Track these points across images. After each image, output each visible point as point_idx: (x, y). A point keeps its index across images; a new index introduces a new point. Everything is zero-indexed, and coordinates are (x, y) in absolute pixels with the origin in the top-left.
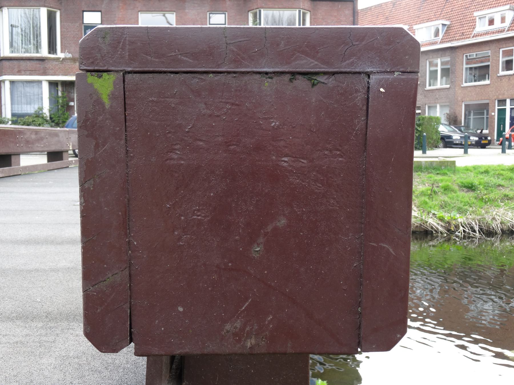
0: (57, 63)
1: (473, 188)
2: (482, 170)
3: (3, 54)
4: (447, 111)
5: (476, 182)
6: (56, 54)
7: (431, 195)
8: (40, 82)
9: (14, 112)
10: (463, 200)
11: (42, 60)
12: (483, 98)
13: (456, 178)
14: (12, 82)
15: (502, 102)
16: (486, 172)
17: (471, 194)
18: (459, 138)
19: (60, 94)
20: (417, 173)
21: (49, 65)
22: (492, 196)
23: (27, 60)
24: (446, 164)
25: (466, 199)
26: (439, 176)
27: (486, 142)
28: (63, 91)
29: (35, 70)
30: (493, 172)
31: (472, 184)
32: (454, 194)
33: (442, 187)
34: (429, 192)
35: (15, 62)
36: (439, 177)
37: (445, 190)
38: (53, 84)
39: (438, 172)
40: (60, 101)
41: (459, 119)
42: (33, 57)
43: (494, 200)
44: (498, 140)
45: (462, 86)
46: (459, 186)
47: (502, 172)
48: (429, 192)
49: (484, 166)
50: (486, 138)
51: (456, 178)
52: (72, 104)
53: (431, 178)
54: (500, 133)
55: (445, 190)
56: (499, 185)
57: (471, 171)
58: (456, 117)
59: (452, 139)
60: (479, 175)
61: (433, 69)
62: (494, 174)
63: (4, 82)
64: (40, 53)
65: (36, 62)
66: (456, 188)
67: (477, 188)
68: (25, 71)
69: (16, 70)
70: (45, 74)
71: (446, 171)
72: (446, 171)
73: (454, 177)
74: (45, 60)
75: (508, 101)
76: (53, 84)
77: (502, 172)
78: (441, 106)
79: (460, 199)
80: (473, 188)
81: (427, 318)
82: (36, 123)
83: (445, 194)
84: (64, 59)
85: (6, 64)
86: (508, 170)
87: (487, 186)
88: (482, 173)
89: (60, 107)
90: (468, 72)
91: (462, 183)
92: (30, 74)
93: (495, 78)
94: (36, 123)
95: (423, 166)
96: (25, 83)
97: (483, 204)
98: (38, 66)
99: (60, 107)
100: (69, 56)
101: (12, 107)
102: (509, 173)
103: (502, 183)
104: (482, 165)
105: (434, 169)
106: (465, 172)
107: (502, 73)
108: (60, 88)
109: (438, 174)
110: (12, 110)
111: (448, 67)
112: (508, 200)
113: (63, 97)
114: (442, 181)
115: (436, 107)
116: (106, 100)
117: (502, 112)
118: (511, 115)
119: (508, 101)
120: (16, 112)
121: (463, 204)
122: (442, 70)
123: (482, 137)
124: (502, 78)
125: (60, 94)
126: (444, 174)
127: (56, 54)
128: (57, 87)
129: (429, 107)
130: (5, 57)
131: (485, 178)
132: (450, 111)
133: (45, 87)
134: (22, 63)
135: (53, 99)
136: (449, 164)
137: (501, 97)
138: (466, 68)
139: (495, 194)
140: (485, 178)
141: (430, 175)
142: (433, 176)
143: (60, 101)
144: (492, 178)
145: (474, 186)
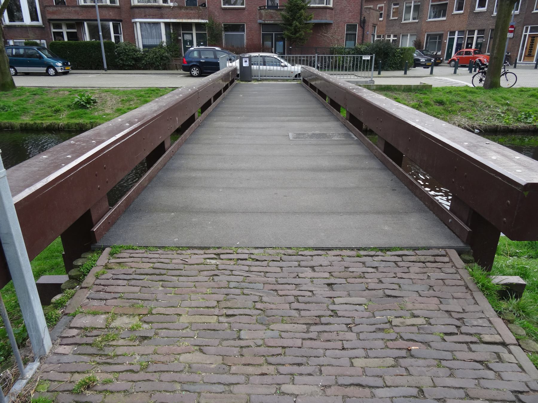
0: (170, 10)
1: (443, 103)
2: (448, 91)
3: (134, 3)
4: (414, 38)
5: (445, 100)
6: (168, 3)
7: (418, 107)
8: (158, 23)
9: (144, 44)
10: (436, 111)
11: (159, 7)
12: (440, 30)
13: (432, 97)
14: (141, 23)
15: (453, 33)
16: (450, 92)
17: (441, 107)
18: (424, 61)
19: (172, 31)
20: (409, 93)
21: (164, 11)
22: (454, 108)
23: (150, 7)
24: (426, 87)
25: (439, 111)
26: (422, 95)
27: (439, 61)
28: (173, 30)
29: (155, 15)
30: (454, 92)
31: (442, 101)
32: (431, 107)
33: (425, 103)
34: (417, 106)
35: (142, 9)
36: (422, 96)
37: (426, 104)
38: (167, 25)
39: (421, 92)
40: (173, 36)
41: (422, 44)
42: (153, 6)
43: (455, 111)
44: (447, 59)
45: (427, 21)
46: (434, 102)
47: (460, 92)
48: (417, 106)
49: (448, 87)
50: (439, 59)
51: (432, 97)
52: (180, 38)
53: (417, 96)
54: (449, 55)
55: (426, 104)
56: (458, 101)
57: (441, 92)
58: (420, 43)
59: (420, 61)
60: (445, 94)
61: (408, 5)
62: (455, 94)
63: (136, 23)
64: (158, 3)
65: (155, 9)
66: (432, 103)
67: (445, 103)
68: (149, 15)
69: (143, 15)
70: (162, 17)
71: (426, 92)
72: (426, 92)
73: (431, 96)
74: (161, 8)
75: (457, 33)
76: (167, 25)
77: (460, 92)
78: (411, 35)
79: (435, 110)
80: (443, 103)
81: (42, 40)
82: (161, 52)
83: (426, 107)
84: (174, 7)
85: (137, 10)
86: (463, 91)
87: (451, 102)
88: (448, 93)
89: (172, 40)
90: (434, 9)
91: (436, 100)
92: (153, 18)
93: (450, 16)
94: (161, 52)
95: (412, 88)
96: (152, 25)
97: (448, 113)
98: (157, 12)
99: (172, 40)
100: (176, 4)
101: (142, 41)
102: (464, 93)
103: (459, 99)
104: (446, 87)
105: (419, 90)
106: (437, 92)
107: (455, 12)
108: (171, 27)
109: (421, 93)
110: (142, 43)
111: (419, 4)
112: (463, 111)
113: (174, 33)
114: (424, 98)
115: (408, 35)
116: (526, 196)
117: (452, 40)
118: (457, 42)
119: (457, 33)
120: (146, 44)
121: (437, 113)
122: (414, 6)
123: (437, 57)
124: (455, 16)
125: (172, 31)
126: (425, 94)
127: (168, 3)
128: (170, 27)
129: (403, 35)
130: (136, 6)
131: (450, 97)
132: (416, 38)
133: (163, 27)
134: (146, 10)
135: (168, 35)
136: (428, 87)
137: (452, 30)
138: (432, 5)
139: (456, 107)
140: (450, 97)
141: (417, 94)
142: (418, 95)
143: (173, 36)
144: (454, 97)
145: (443, 102)
